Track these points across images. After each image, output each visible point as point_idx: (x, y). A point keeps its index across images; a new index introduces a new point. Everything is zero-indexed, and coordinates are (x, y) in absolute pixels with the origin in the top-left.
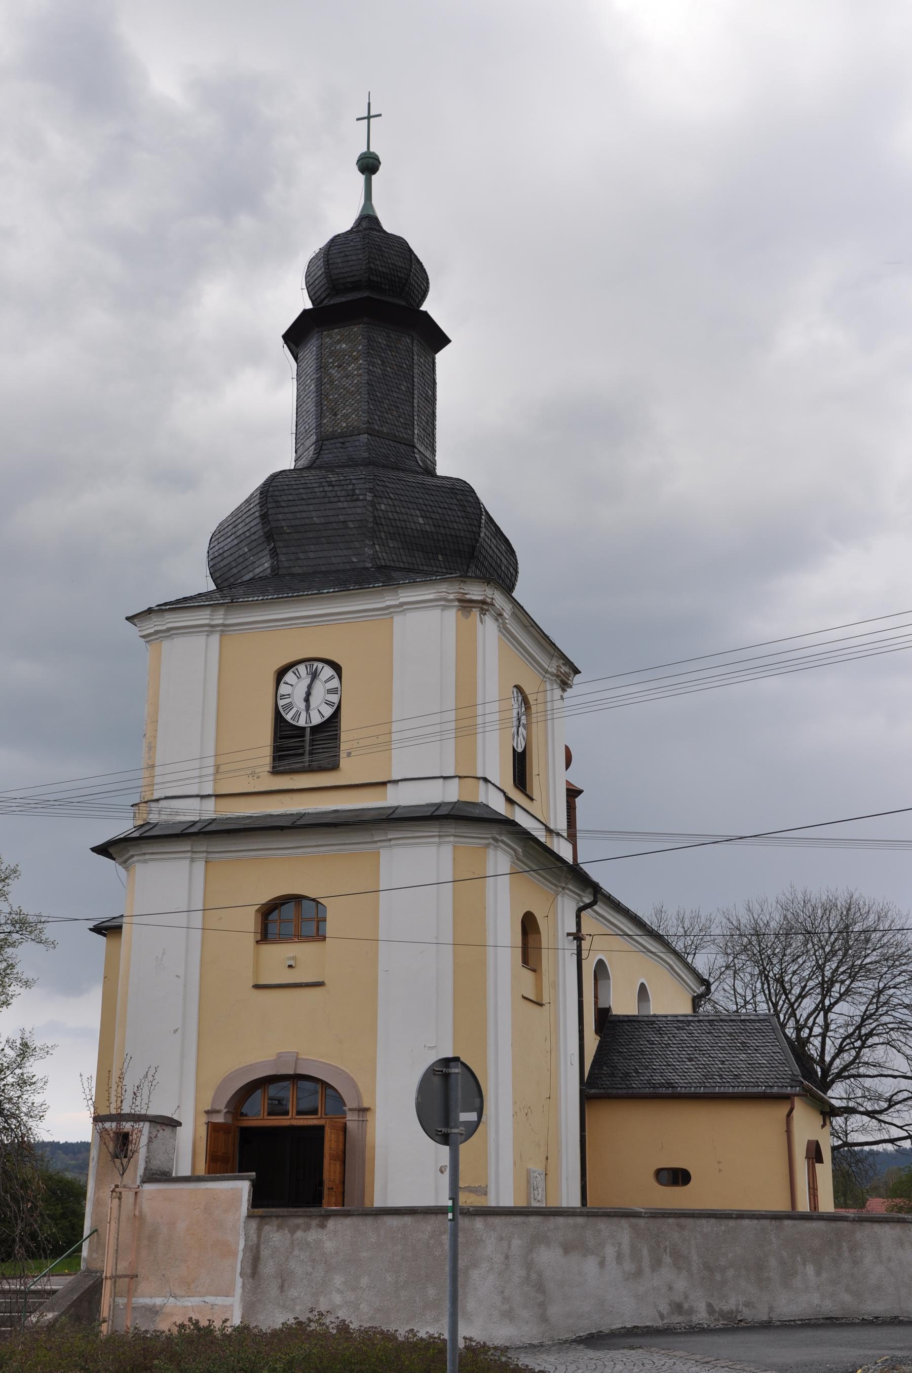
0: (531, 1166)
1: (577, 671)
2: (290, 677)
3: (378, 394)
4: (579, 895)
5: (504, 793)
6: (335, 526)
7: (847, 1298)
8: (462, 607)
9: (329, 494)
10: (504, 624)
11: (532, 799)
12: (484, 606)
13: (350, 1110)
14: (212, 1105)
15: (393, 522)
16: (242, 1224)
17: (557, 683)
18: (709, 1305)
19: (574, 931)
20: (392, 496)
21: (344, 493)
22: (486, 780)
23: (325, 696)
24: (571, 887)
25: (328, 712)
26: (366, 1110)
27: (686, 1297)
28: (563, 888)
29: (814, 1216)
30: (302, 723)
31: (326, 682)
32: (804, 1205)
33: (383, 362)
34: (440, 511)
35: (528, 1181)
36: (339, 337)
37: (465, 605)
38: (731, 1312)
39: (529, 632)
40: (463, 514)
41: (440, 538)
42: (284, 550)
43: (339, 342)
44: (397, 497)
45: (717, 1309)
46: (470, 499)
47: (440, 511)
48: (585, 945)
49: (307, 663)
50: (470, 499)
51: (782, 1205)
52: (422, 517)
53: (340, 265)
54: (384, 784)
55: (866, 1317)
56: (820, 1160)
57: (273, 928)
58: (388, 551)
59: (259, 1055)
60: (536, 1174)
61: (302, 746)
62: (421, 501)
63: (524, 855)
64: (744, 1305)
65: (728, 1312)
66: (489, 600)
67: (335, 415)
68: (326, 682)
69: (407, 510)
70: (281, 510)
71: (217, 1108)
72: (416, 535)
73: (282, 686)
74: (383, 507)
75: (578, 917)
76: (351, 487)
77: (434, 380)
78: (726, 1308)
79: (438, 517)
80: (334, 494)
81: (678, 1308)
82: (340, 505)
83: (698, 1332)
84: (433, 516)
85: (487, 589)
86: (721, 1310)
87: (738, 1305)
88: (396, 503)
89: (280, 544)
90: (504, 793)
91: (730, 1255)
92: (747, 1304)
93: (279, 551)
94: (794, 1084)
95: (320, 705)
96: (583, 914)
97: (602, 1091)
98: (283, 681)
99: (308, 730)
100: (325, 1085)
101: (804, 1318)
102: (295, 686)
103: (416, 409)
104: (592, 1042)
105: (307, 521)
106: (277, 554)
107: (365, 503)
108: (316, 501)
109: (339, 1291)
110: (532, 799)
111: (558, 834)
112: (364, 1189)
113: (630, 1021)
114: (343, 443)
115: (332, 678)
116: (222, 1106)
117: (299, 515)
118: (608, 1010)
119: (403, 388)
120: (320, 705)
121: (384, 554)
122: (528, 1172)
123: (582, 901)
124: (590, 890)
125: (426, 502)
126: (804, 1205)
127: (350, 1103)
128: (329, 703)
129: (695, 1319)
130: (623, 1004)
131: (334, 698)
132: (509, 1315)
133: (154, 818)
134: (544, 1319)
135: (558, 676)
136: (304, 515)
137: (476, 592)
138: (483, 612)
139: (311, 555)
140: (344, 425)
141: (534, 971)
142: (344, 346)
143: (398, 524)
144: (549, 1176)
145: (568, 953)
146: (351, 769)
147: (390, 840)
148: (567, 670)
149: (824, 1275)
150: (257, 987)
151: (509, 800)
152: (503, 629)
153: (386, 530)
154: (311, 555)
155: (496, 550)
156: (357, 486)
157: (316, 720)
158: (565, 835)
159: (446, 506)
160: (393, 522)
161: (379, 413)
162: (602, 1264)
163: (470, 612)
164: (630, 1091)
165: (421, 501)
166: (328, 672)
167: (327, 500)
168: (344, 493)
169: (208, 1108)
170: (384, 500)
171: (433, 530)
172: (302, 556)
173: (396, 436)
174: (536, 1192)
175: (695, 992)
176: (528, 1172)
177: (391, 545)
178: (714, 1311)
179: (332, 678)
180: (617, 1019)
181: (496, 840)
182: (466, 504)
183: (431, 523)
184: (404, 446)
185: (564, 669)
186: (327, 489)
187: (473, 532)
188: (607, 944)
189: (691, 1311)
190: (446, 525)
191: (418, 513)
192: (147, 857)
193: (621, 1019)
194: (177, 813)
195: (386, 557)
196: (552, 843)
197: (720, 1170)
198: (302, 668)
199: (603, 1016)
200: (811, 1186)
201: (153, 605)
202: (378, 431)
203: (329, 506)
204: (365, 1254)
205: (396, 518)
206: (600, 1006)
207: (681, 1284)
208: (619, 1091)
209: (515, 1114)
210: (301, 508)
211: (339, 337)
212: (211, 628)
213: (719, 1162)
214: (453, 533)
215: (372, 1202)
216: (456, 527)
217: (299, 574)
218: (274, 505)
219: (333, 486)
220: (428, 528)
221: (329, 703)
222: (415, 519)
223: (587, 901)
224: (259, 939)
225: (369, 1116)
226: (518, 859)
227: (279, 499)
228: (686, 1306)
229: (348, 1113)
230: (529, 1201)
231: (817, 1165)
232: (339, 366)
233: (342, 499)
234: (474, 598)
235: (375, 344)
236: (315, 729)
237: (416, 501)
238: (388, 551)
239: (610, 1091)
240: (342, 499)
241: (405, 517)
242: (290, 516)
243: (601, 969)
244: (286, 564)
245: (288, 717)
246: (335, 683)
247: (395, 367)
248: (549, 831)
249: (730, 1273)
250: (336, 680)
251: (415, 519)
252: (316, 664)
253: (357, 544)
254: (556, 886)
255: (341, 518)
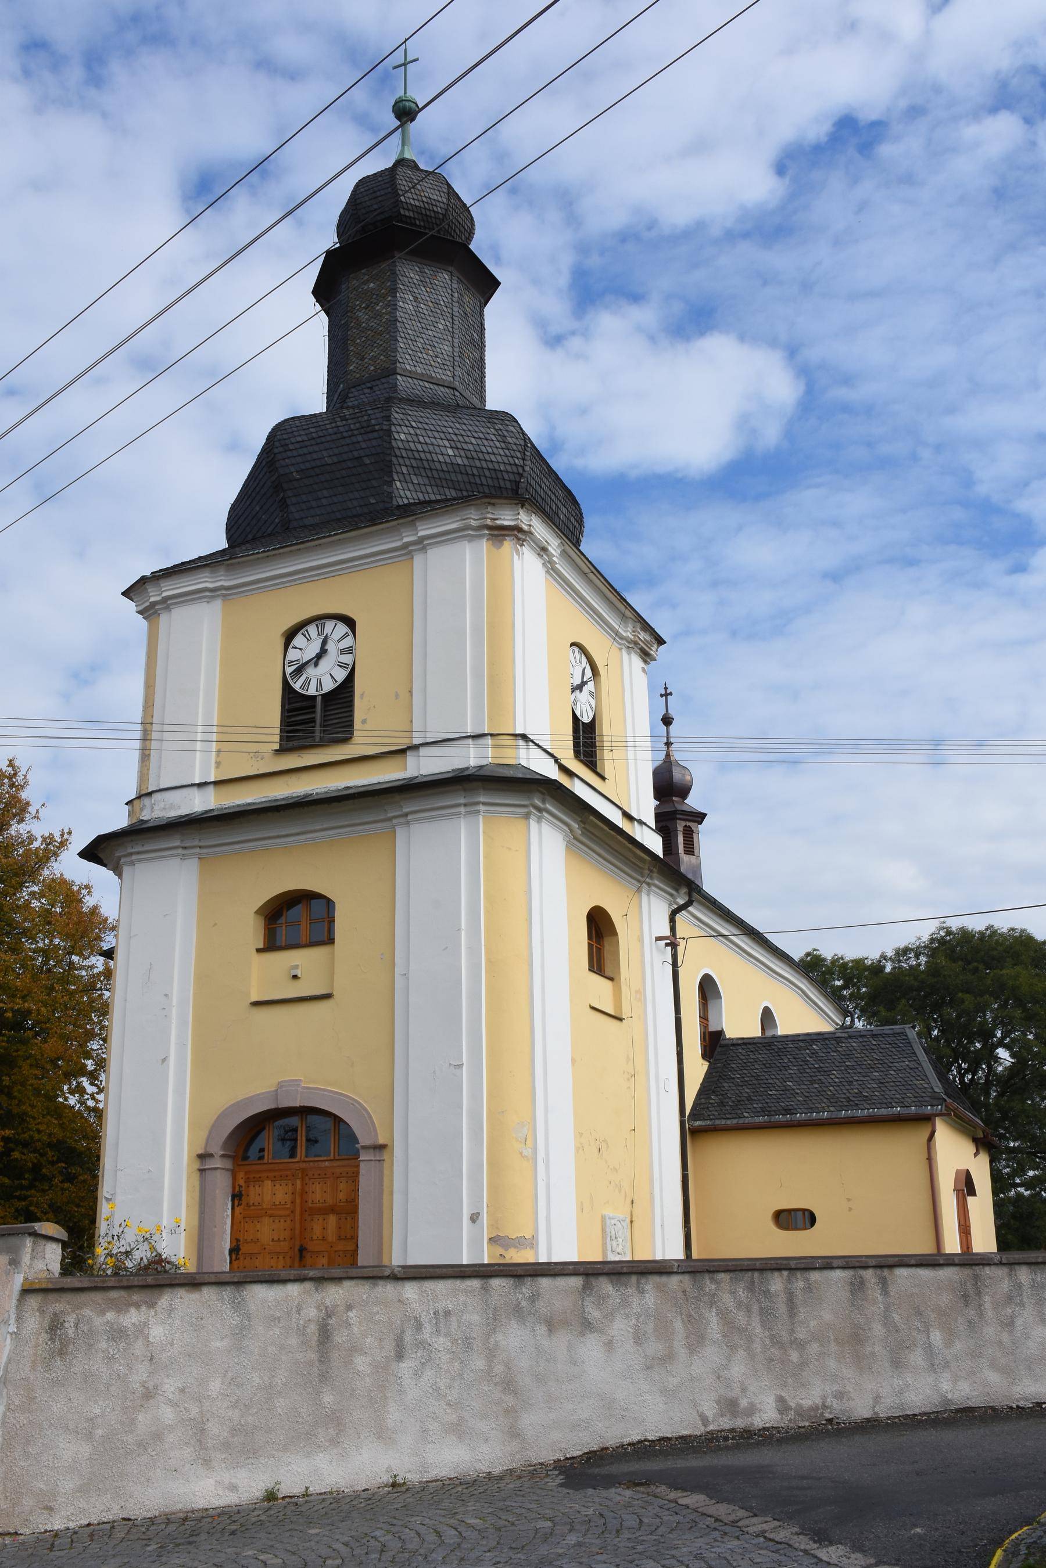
0: (608, 1212)
1: (661, 641)
2: (299, 640)
3: (410, 332)
4: (671, 895)
5: (556, 761)
6: (349, 464)
7: (993, 1377)
8: (492, 535)
9: (342, 429)
10: (551, 562)
11: (603, 778)
12: (518, 533)
13: (364, 1147)
14: (206, 1148)
15: (416, 454)
16: (14, 1302)
17: (636, 652)
18: (781, 1400)
19: (668, 933)
20: (414, 424)
21: (358, 425)
22: (524, 737)
23: (337, 657)
24: (656, 882)
25: (341, 675)
26: (382, 1147)
27: (744, 1389)
28: (648, 884)
29: (968, 1260)
30: (312, 691)
31: (339, 641)
32: (952, 1245)
33: (416, 299)
34: (473, 441)
35: (604, 1230)
36: (367, 277)
37: (496, 533)
38: (815, 1408)
39: (590, 582)
40: (503, 445)
41: (475, 472)
42: (294, 500)
43: (368, 281)
44: (420, 425)
45: (793, 1405)
46: (512, 428)
47: (473, 441)
48: (680, 950)
49: (317, 622)
50: (512, 428)
51: (924, 1247)
52: (451, 447)
53: (368, 203)
54: (402, 752)
55: (1021, 1404)
56: (972, 1192)
57: (282, 936)
58: (411, 488)
59: (254, 1087)
60: (613, 1222)
61: (315, 718)
62: (450, 430)
63: (583, 834)
64: (835, 1397)
65: (811, 1409)
66: (525, 528)
67: (363, 359)
68: (339, 641)
69: (433, 440)
70: (289, 454)
71: (211, 1151)
72: (445, 469)
73: (291, 651)
74: (403, 436)
75: (672, 920)
76: (366, 418)
77: (482, 325)
78: (807, 1403)
79: (471, 447)
80: (347, 428)
81: (731, 1406)
82: (354, 439)
83: (758, 1444)
84: (465, 446)
85: (521, 511)
86: (799, 1406)
87: (824, 1398)
88: (418, 432)
89: (290, 493)
90: (556, 761)
91: (812, 1324)
92: (840, 1395)
93: (289, 502)
94: (935, 1102)
95: (332, 669)
96: (678, 917)
97: (708, 1122)
98: (337, 685)
99: (319, 699)
100: (337, 1120)
101: (928, 1410)
102: (305, 647)
103: (457, 350)
104: (697, 1069)
105: (318, 463)
106: (287, 506)
107: (381, 433)
108: (329, 438)
109: (170, 1402)
110: (603, 778)
111: (641, 822)
112: (380, 1243)
113: (744, 1044)
114: (371, 388)
115: (346, 635)
116: (217, 1150)
117: (309, 457)
118: (721, 1033)
119: (441, 326)
120: (332, 669)
121: (408, 493)
122: (603, 1218)
123: (676, 903)
124: (684, 890)
125: (457, 432)
126: (952, 1245)
127: (363, 1140)
128: (343, 665)
129: (758, 1422)
130: (739, 1023)
131: (347, 659)
132: (458, 1430)
133: (146, 816)
134: (514, 1433)
135: (636, 643)
136: (315, 456)
137: (506, 518)
138: (521, 542)
139: (325, 502)
140: (372, 368)
141: (611, 979)
142: (372, 285)
143: (422, 455)
144: (634, 1224)
145: (657, 964)
146: (360, 745)
147: (406, 815)
148: (648, 638)
149: (958, 1346)
150: (417, 60)
151: (563, 769)
152: (551, 569)
153: (408, 463)
154: (325, 502)
155: (548, 492)
156: (373, 417)
157: (328, 686)
158: (652, 824)
159: (481, 436)
160: (416, 454)
161: (411, 352)
162: (609, 1345)
163: (501, 542)
164: (741, 1121)
165: (450, 430)
166: (342, 629)
167: (339, 436)
168: (358, 425)
169: (201, 1152)
170: (404, 428)
171: (466, 462)
172: (314, 504)
173: (432, 377)
174: (614, 1243)
175: (837, 1024)
176: (603, 1218)
177: (415, 481)
178: (790, 1408)
179: (346, 635)
180: (730, 1042)
181: (540, 810)
182: (505, 433)
183: (463, 454)
184: (442, 389)
185: (643, 636)
186: (339, 424)
187: (516, 465)
188: (706, 954)
189: (751, 1410)
190: (482, 457)
191: (447, 443)
192: (134, 857)
193: (735, 1042)
194: (172, 807)
195: (409, 496)
196: (634, 831)
197: (850, 1209)
198: (312, 629)
199: (714, 1043)
200: (962, 1223)
201: (148, 573)
202: (410, 372)
203: (343, 442)
204: (219, 1344)
205: (420, 449)
206: (712, 1028)
207: (738, 1370)
208: (729, 1122)
209: (580, 1148)
210: (311, 449)
211: (367, 277)
212: (213, 593)
213: (849, 1200)
214: (491, 466)
215: (391, 1260)
216: (494, 459)
217: (311, 525)
218: (281, 449)
219: (347, 420)
220: (459, 461)
221: (343, 665)
222: (443, 449)
223: (681, 902)
224: (261, 946)
225: (386, 1156)
226: (575, 838)
227: (287, 442)
228: (744, 1403)
229: (361, 1152)
230: (605, 1254)
231: (970, 1199)
232: (365, 308)
233: (356, 432)
234: (507, 523)
235: (406, 279)
236: (328, 697)
237: (444, 429)
238: (411, 488)
239: (717, 1122)
240: (356, 432)
241: (431, 448)
242: (299, 460)
243: (708, 988)
244: (297, 516)
245: (297, 686)
246: (348, 642)
247: (431, 304)
248: (627, 816)
249: (814, 1348)
250: (351, 637)
251: (443, 449)
252: (329, 625)
253: (374, 483)
254: (639, 881)
255: (356, 454)
